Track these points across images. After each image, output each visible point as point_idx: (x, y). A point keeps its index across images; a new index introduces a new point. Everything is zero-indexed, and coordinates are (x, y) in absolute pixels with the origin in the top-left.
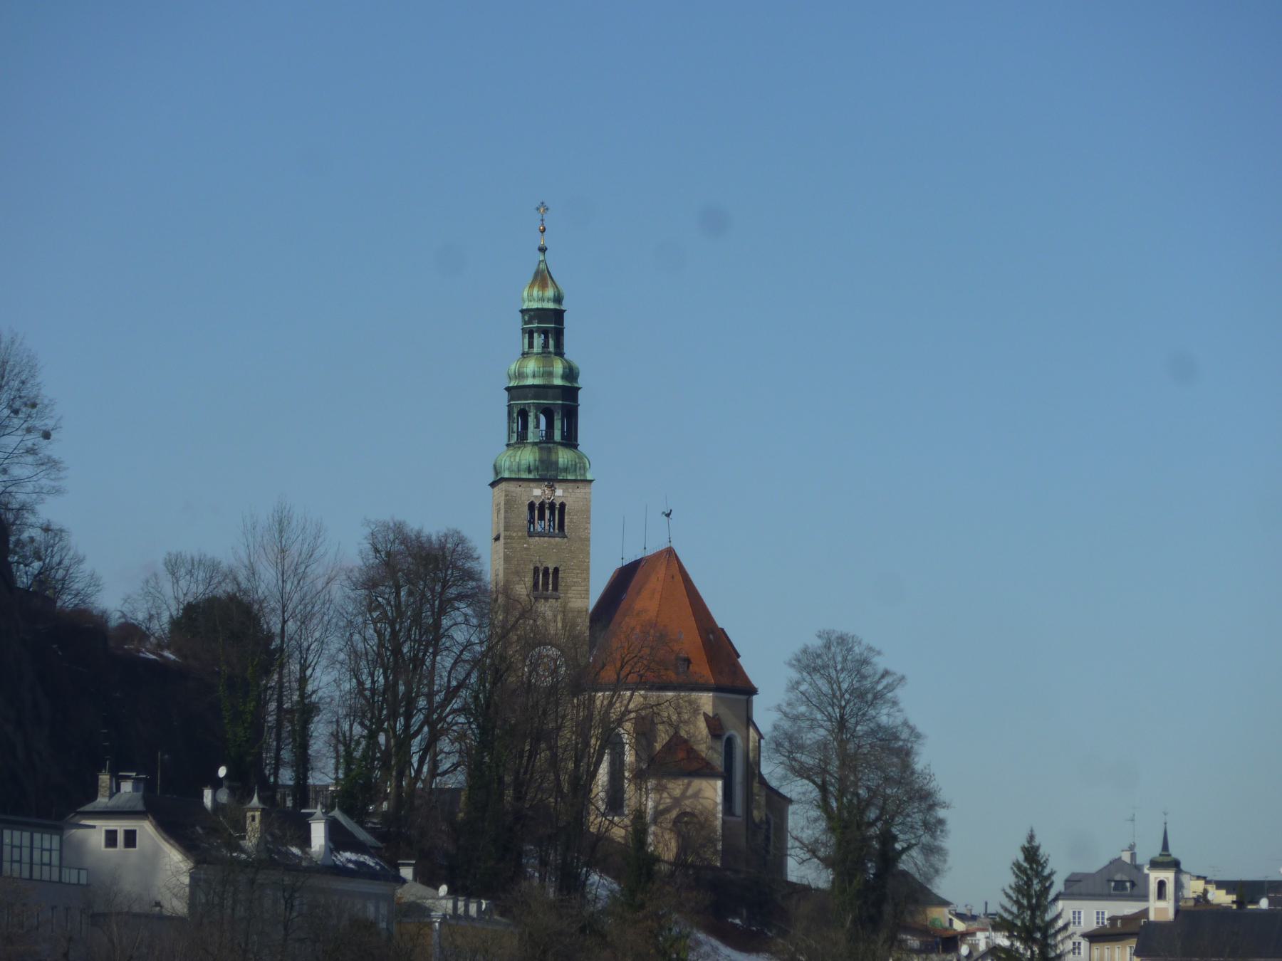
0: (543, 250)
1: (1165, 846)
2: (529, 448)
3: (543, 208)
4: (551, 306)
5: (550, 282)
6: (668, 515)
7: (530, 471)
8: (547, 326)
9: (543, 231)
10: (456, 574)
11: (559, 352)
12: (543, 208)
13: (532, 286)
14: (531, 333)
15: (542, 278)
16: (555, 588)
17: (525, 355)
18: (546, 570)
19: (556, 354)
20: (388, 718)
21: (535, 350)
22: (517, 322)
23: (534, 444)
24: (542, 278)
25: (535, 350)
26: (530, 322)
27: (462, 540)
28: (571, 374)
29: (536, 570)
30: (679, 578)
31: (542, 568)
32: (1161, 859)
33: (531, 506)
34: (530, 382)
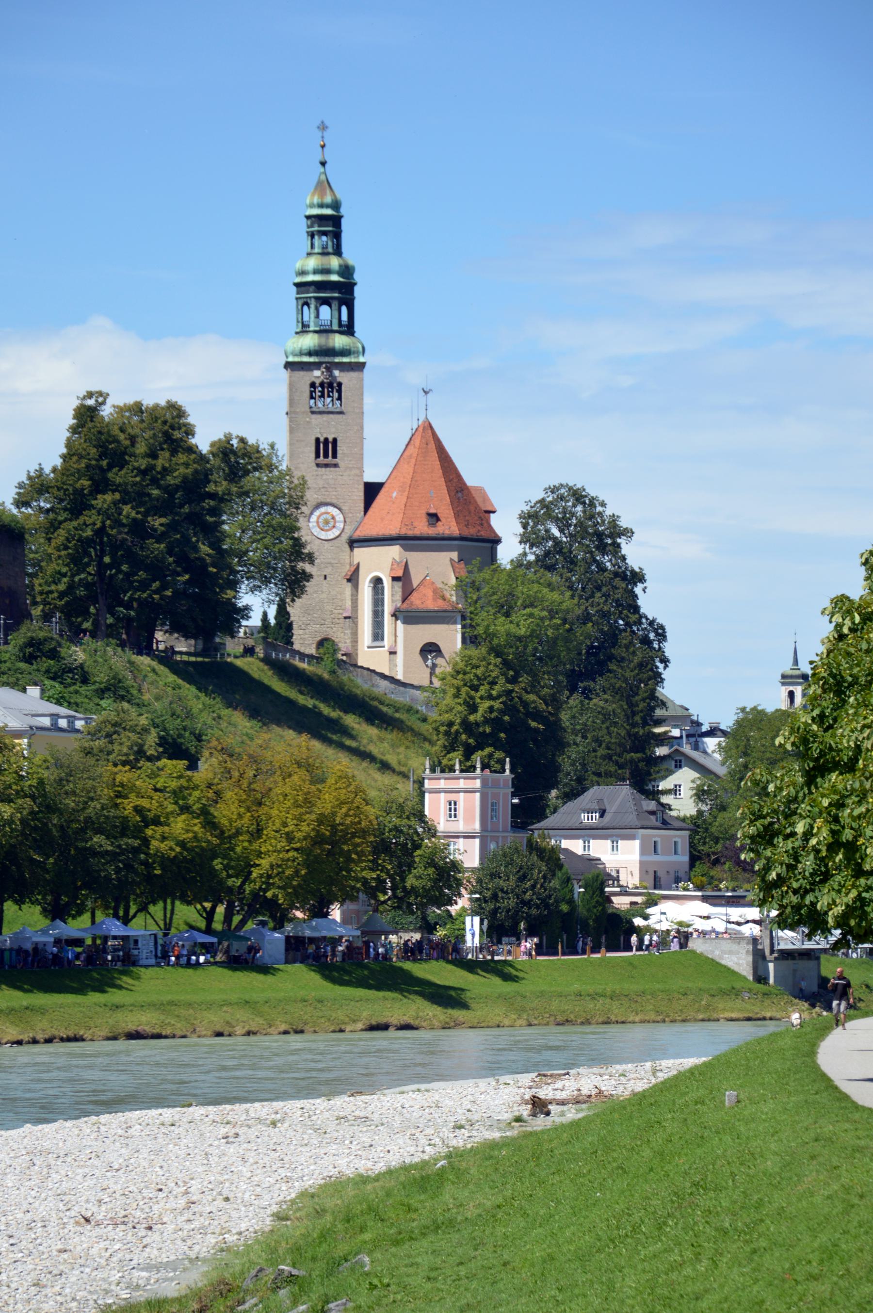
0: (323, 164)
1: (796, 662)
2: (311, 335)
3: (323, 127)
4: (329, 212)
5: (328, 191)
6: (426, 393)
7: (310, 354)
8: (328, 226)
9: (323, 147)
10: (655, 938)
11: (338, 252)
12: (323, 127)
13: (313, 195)
14: (312, 235)
15: (324, 185)
16: (335, 456)
17: (309, 254)
18: (326, 440)
19: (334, 254)
20: (182, 956)
21: (316, 250)
22: (303, 226)
23: (315, 332)
24: (324, 185)
25: (316, 250)
26: (312, 226)
27: (512, 561)
28: (347, 271)
29: (317, 440)
30: (432, 445)
31: (322, 439)
32: (791, 672)
33: (313, 385)
34: (311, 278)
